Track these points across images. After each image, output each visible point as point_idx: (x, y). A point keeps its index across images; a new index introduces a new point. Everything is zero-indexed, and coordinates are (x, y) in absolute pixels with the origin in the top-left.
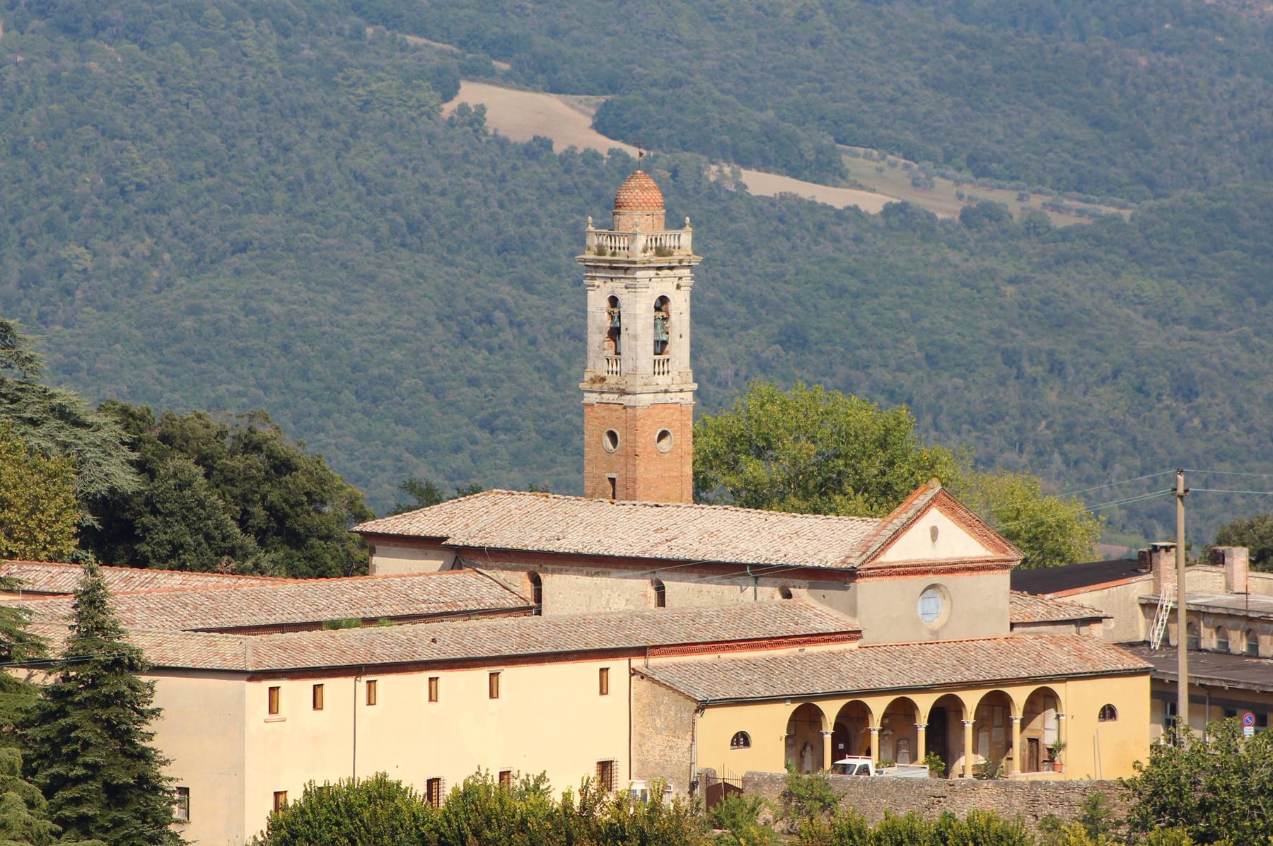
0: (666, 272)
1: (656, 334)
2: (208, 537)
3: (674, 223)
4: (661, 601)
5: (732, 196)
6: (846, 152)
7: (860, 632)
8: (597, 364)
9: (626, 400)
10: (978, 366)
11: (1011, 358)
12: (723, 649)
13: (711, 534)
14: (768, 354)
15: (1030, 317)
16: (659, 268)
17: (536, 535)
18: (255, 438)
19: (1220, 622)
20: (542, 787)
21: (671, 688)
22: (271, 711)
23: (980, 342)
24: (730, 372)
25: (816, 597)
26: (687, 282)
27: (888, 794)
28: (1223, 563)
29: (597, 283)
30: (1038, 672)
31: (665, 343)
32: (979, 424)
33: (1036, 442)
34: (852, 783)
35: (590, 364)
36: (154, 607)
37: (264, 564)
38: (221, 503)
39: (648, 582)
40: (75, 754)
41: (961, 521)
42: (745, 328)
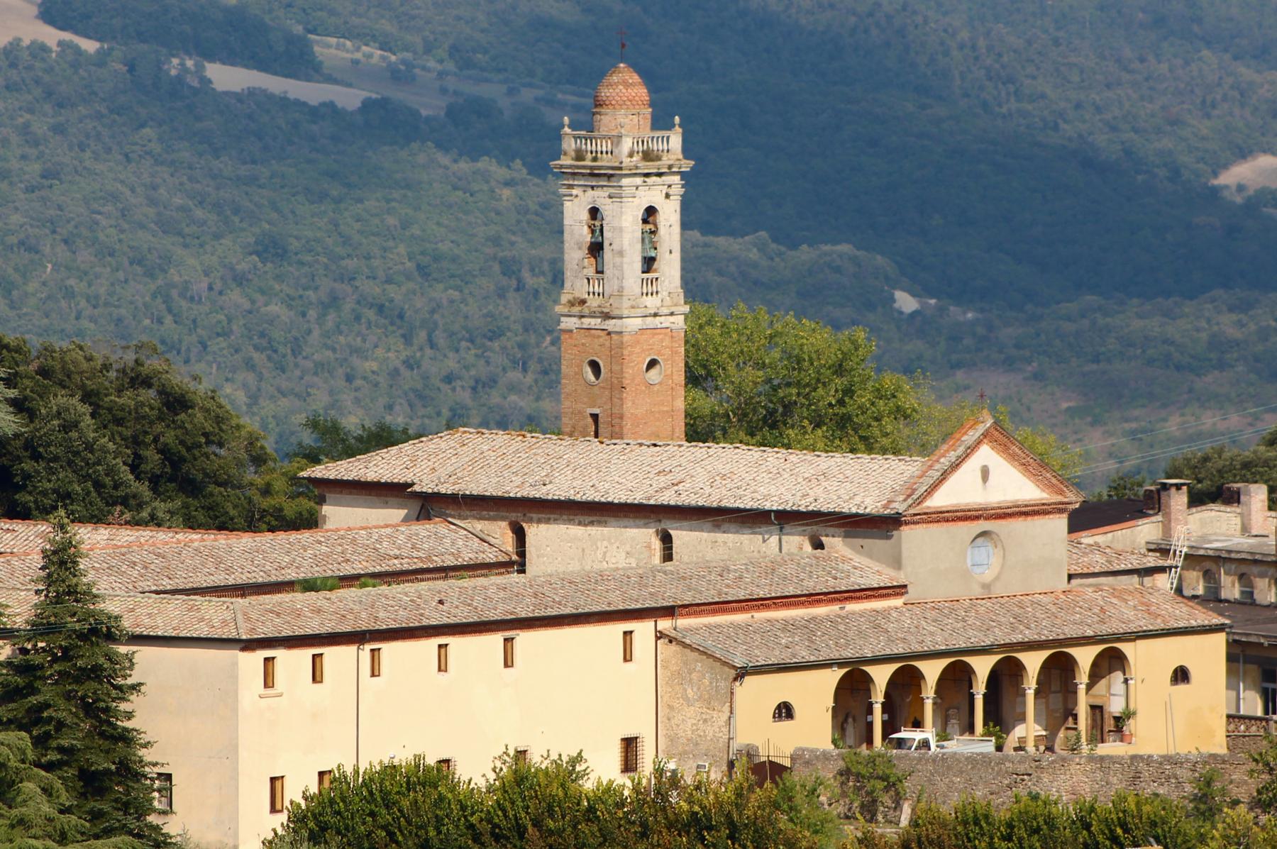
0: (654, 179)
1: (643, 250)
2: (98, 485)
3: (660, 122)
4: (668, 556)
5: (195, 92)
6: (317, 42)
7: (905, 586)
8: (576, 284)
9: (611, 325)
10: (475, 276)
11: (510, 268)
12: (758, 608)
13: (724, 477)
14: (242, 267)
15: (529, 223)
16: (647, 175)
17: (518, 480)
18: (145, 370)
19: (1244, 569)
20: (578, 768)
21: (705, 653)
22: (266, 686)
23: (476, 251)
24: (204, 285)
25: (853, 548)
26: (677, 190)
27: (962, 772)
28: (1239, 502)
29: (574, 192)
30: (1104, 629)
31: (653, 259)
32: (478, 341)
33: (540, 360)
34: (920, 760)
35: (567, 284)
36: (128, 563)
37: (160, 514)
38: (111, 446)
39: (652, 531)
40: (47, 736)
41: (1012, 458)
42: (217, 237)
